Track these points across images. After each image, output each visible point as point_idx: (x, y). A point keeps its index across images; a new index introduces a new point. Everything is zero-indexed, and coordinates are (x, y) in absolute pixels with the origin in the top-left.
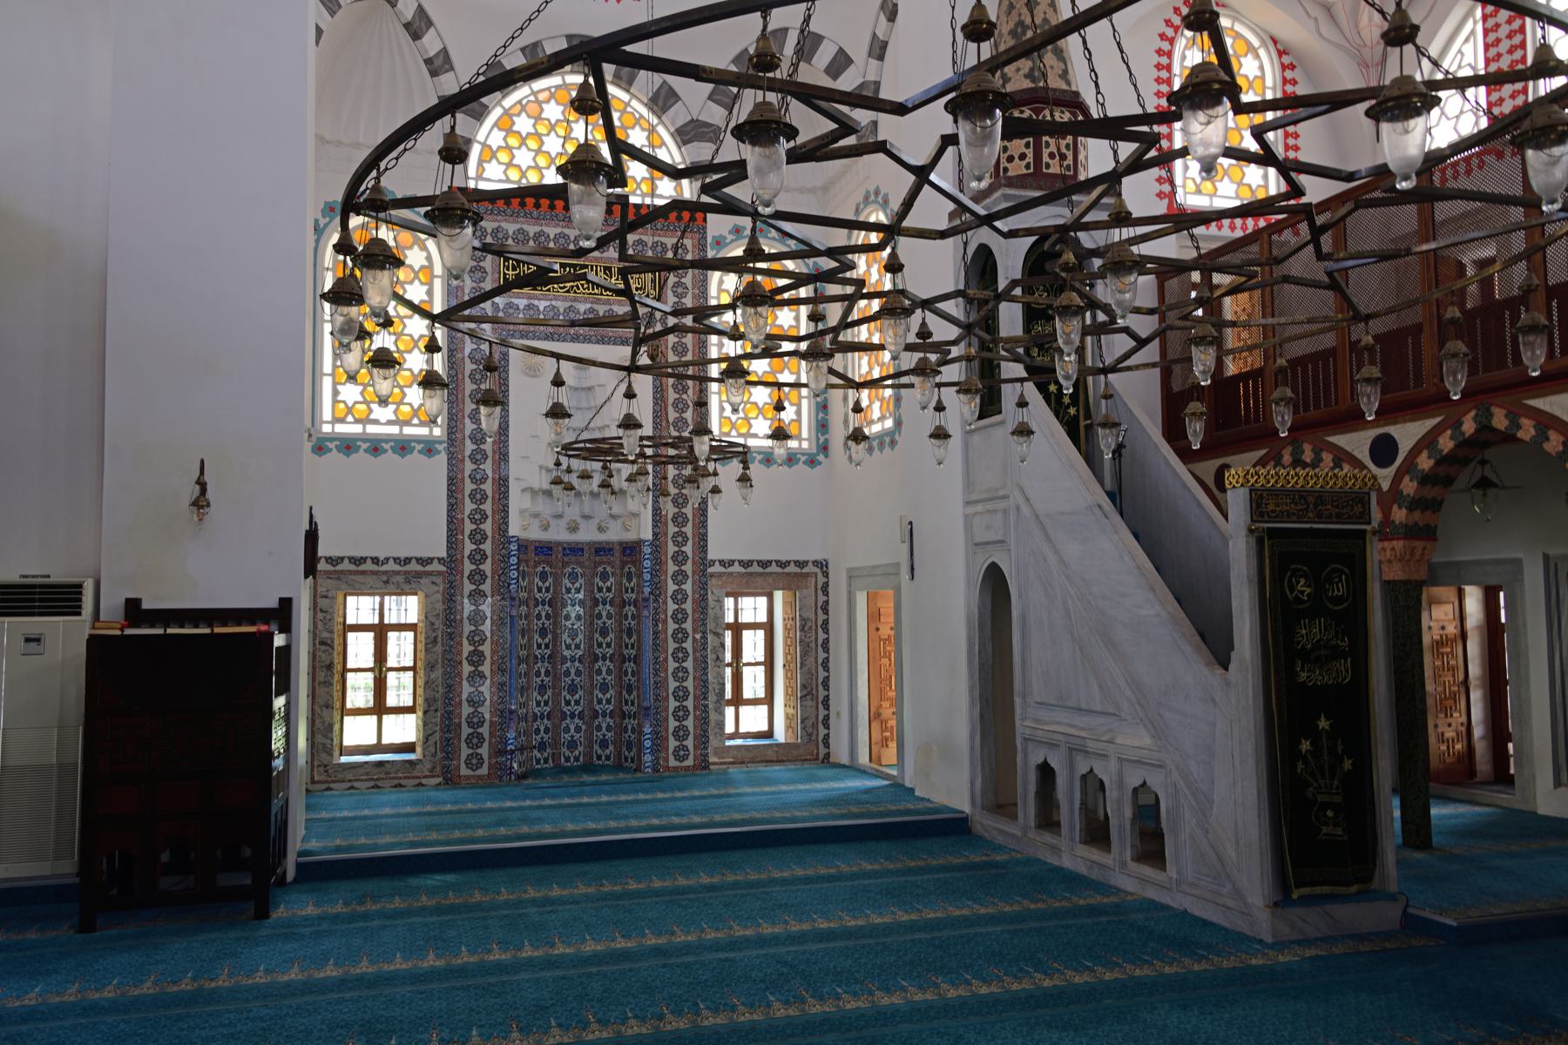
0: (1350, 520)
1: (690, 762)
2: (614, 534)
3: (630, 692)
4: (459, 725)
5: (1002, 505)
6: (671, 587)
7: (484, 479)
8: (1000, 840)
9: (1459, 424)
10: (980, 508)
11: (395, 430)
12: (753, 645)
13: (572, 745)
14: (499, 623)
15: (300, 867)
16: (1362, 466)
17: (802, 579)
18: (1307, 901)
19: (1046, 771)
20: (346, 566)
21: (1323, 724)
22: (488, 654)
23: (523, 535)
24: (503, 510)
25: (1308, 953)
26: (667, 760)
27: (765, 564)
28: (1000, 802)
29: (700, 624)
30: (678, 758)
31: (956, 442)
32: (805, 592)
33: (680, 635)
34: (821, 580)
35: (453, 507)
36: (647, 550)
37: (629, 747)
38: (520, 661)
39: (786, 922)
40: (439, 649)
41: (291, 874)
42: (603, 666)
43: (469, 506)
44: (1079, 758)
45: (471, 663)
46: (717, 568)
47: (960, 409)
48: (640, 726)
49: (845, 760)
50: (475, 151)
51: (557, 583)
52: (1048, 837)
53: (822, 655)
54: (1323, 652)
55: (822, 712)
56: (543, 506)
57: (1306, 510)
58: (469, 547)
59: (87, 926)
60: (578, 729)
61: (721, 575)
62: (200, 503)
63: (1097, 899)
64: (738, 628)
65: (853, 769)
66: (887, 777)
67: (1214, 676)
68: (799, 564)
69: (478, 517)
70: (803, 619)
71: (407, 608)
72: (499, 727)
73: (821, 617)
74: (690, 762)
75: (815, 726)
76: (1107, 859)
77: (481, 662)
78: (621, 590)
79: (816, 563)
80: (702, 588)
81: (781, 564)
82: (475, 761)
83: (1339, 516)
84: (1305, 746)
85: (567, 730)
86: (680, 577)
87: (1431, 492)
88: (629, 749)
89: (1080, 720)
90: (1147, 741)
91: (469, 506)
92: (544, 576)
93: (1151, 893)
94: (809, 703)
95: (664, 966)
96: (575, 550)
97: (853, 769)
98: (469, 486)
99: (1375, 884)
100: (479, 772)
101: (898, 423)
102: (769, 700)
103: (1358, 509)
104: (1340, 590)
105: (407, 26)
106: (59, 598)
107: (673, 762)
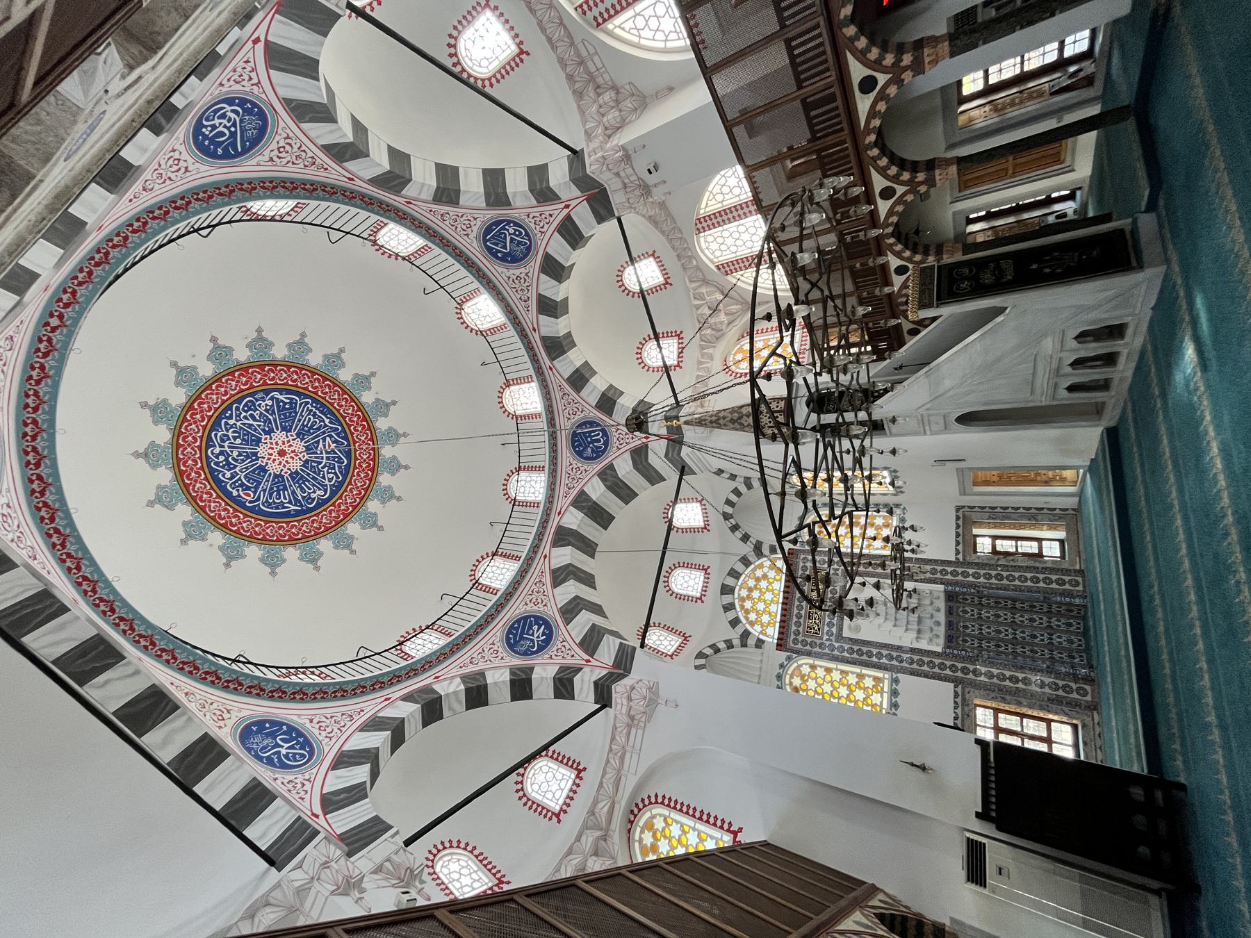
0: (932, 276)
2: (941, 604)
5: (926, 419)
6: (971, 579)
8: (1118, 411)
9: (891, 245)
12: (1005, 546)
14: (992, 664)
16: (908, 279)
17: (966, 520)
19: (1072, 388)
21: (1034, 266)
25: (1171, 247)
27: (958, 535)
28: (1098, 411)
29: (991, 567)
30: (1077, 584)
35: (926, 675)
40: (1008, 697)
43: (925, 668)
44: (1062, 372)
46: (960, 557)
47: (880, 442)
48: (1056, 603)
49: (1077, 499)
50: (762, 637)
51: (969, 635)
52: (1115, 383)
56: (927, 635)
59: (1197, 889)
62: (923, 768)
64: (995, 551)
66: (1084, 475)
68: (958, 518)
70: (989, 518)
72: (1058, 675)
74: (1080, 579)
75: (1054, 515)
76: (1125, 352)
77: (1017, 678)
78: (972, 604)
80: (970, 565)
81: (958, 527)
84: (1047, 270)
86: (965, 574)
87: (920, 248)
90: (1049, 339)
93: (1144, 327)
96: (950, 625)
97: (1081, 494)
98: (915, 666)
101: (886, 468)
102: (1039, 540)
104: (966, 271)
107: (1080, 588)
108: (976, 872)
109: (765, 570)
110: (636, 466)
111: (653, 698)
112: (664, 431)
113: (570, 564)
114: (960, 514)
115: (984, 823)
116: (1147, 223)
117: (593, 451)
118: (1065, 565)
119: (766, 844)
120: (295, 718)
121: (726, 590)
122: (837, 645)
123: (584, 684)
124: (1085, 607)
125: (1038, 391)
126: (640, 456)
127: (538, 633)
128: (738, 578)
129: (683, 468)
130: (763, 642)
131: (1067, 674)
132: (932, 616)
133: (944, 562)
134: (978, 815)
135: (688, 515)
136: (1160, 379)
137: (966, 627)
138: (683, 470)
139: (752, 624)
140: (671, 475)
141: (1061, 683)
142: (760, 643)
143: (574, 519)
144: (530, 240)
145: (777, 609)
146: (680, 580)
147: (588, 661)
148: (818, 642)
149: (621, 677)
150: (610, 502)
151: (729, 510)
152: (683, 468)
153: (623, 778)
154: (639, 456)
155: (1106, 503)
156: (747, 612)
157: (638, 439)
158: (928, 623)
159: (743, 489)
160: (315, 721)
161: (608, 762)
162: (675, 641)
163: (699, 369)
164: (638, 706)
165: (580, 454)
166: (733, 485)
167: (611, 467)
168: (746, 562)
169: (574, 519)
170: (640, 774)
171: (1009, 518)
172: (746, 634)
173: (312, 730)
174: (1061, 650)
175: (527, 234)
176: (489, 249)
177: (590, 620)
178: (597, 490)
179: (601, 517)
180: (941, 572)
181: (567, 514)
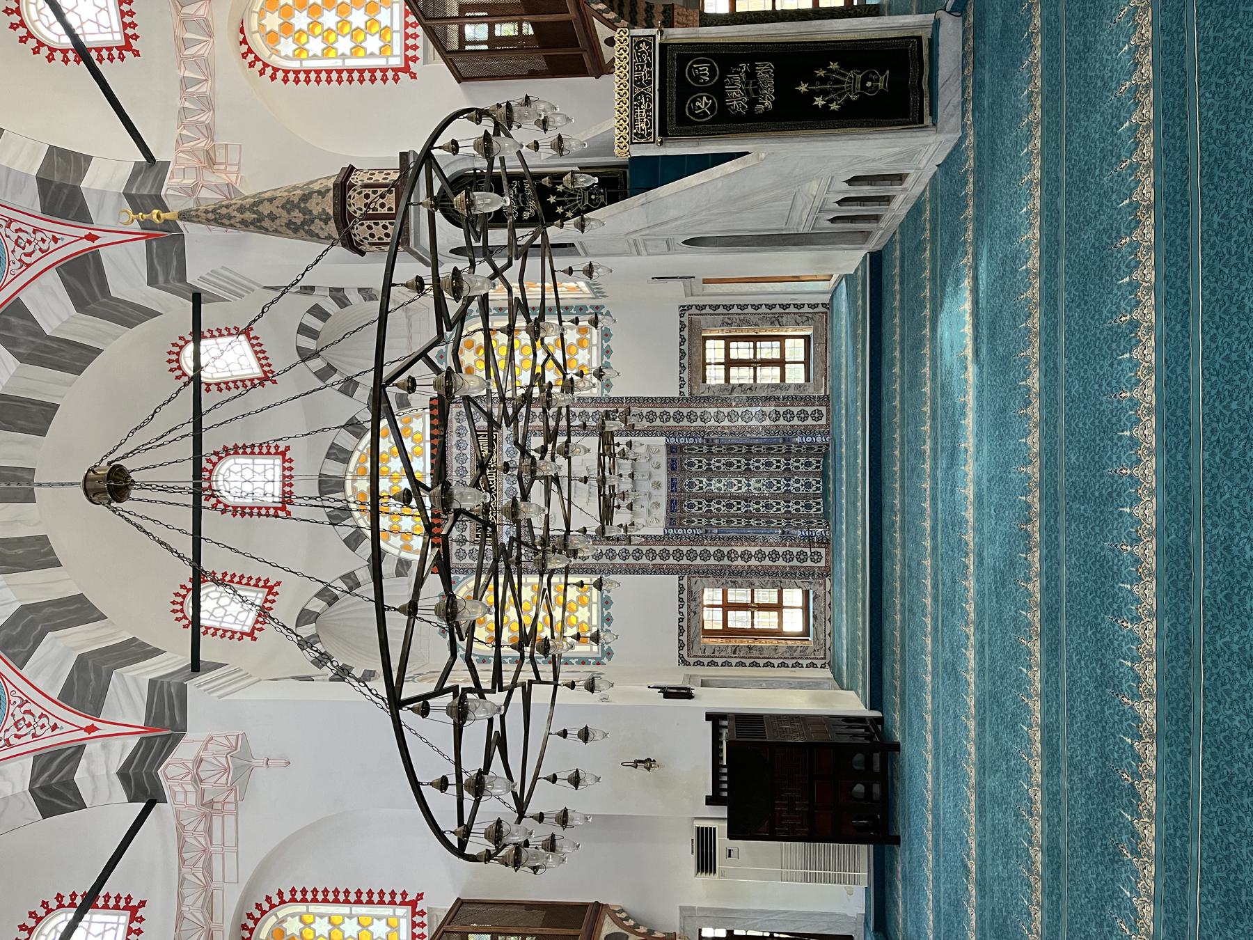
1: (823, 409)
2: (662, 459)
4: (791, 567)
7: (626, 551)
11: (594, 607)
13: (808, 485)
15: (872, 708)
18: (933, 113)
19: (833, 220)
20: (684, 638)
21: (803, 88)
22: (743, 549)
23: (663, 523)
26: (821, 426)
31: (595, 261)
32: (703, 323)
34: (694, 311)
36: (672, 441)
38: (749, 525)
39: (966, 218)
40: (739, 580)
41: (877, 714)
43: (644, 561)
45: (749, 559)
46: (686, 390)
51: (695, 496)
53: (749, 310)
54: (750, 87)
55: (792, 309)
57: (645, 94)
58: (671, 561)
59: (897, 841)
60: (797, 481)
61: (690, 387)
62: (648, 763)
69: (651, 554)
71: (712, 595)
73: (721, 310)
74: (823, 409)
75: (801, 315)
77: (749, 554)
82: (816, 557)
83: (649, 65)
84: (819, 102)
85: (797, 489)
88: (813, 449)
91: (644, 561)
92: (691, 506)
94: (784, 319)
96: (673, 484)
97: (834, 292)
98: (631, 561)
99: (926, 35)
100: (823, 554)
102: (781, 339)
103: (643, 47)
105: (330, 605)
107: (823, 422)
108: (706, 863)
110: (81, 304)
111: (241, 763)
112: (136, 227)
118: (810, 391)
123: (97, 774)
126: (85, 281)
128: (346, 461)
131: (803, 538)
135: (227, 359)
136: (933, 298)
147: (90, 729)
149: (170, 742)
153: (218, 895)
154: (83, 278)
159: (330, 306)
163: (182, 61)
164: (215, 784)
166: (310, 301)
170: (246, 877)
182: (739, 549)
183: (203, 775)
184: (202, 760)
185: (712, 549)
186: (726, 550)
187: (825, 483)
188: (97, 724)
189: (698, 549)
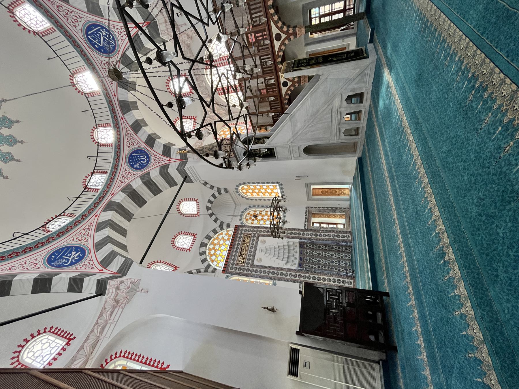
1: (350, 235)
2: (298, 249)
3: (333, 248)
6: (310, 236)
8: (362, 147)
10: (292, 155)
13: (346, 264)
17: (310, 213)
24: (290, 270)
30: (349, 237)
33: (320, 235)
36: (301, 241)
37: (346, 249)
42: (327, 255)
43: (288, 277)
45: (325, 281)
46: (306, 227)
50: (216, 267)
51: (308, 263)
56: (291, 263)
58: (297, 278)
60: (342, 262)
62: (272, 310)
63: (372, 105)
65: (350, 200)
67: (322, 79)
68: (306, 211)
69: (291, 275)
70: (318, 211)
72: (341, 276)
74: (350, 235)
76: (363, 110)
77: (325, 279)
79: (306, 208)
81: (306, 215)
89: (334, 122)
95: (386, 132)
96: (301, 259)
97: (350, 200)
101: (278, 183)
106: (294, 354)
107: (350, 239)
109: (224, 235)
110: (161, 174)
113: (110, 220)
114: (307, 210)
115: (301, 338)
116: (370, 47)
117: (140, 165)
118: (345, 230)
119: (181, 372)
120: (65, 243)
121: (203, 245)
122: (250, 269)
124: (351, 247)
125: (333, 134)
127: (74, 255)
128: (210, 239)
129: (186, 177)
130: (216, 269)
132: (294, 255)
133: (299, 230)
134: (297, 333)
137: (307, 260)
138: (186, 179)
139: (213, 261)
140: (179, 179)
141: (342, 280)
142: (214, 270)
143: (120, 198)
144: (115, 42)
145: (225, 253)
146: (181, 241)
148: (242, 268)
150: (145, 192)
151: (209, 205)
152: (186, 177)
154: (164, 171)
155: (358, 187)
156: (212, 255)
157: (165, 160)
158: (292, 258)
160: (75, 239)
161: (92, 331)
162: (190, 239)
164: (122, 294)
165: (132, 166)
166: (212, 192)
167: (148, 174)
168: (215, 232)
169: (120, 198)
171: (325, 212)
172: (209, 266)
173: (76, 243)
174: (343, 267)
175: (113, 38)
176: (90, 41)
177: (111, 248)
178: (137, 184)
179: (140, 201)
180: (298, 234)
181: (118, 195)
182: (321, 277)
183: (121, 287)
184: (123, 282)
185: (312, 276)
186: (317, 276)
187: (352, 264)
188: (104, 269)
189: (307, 275)
